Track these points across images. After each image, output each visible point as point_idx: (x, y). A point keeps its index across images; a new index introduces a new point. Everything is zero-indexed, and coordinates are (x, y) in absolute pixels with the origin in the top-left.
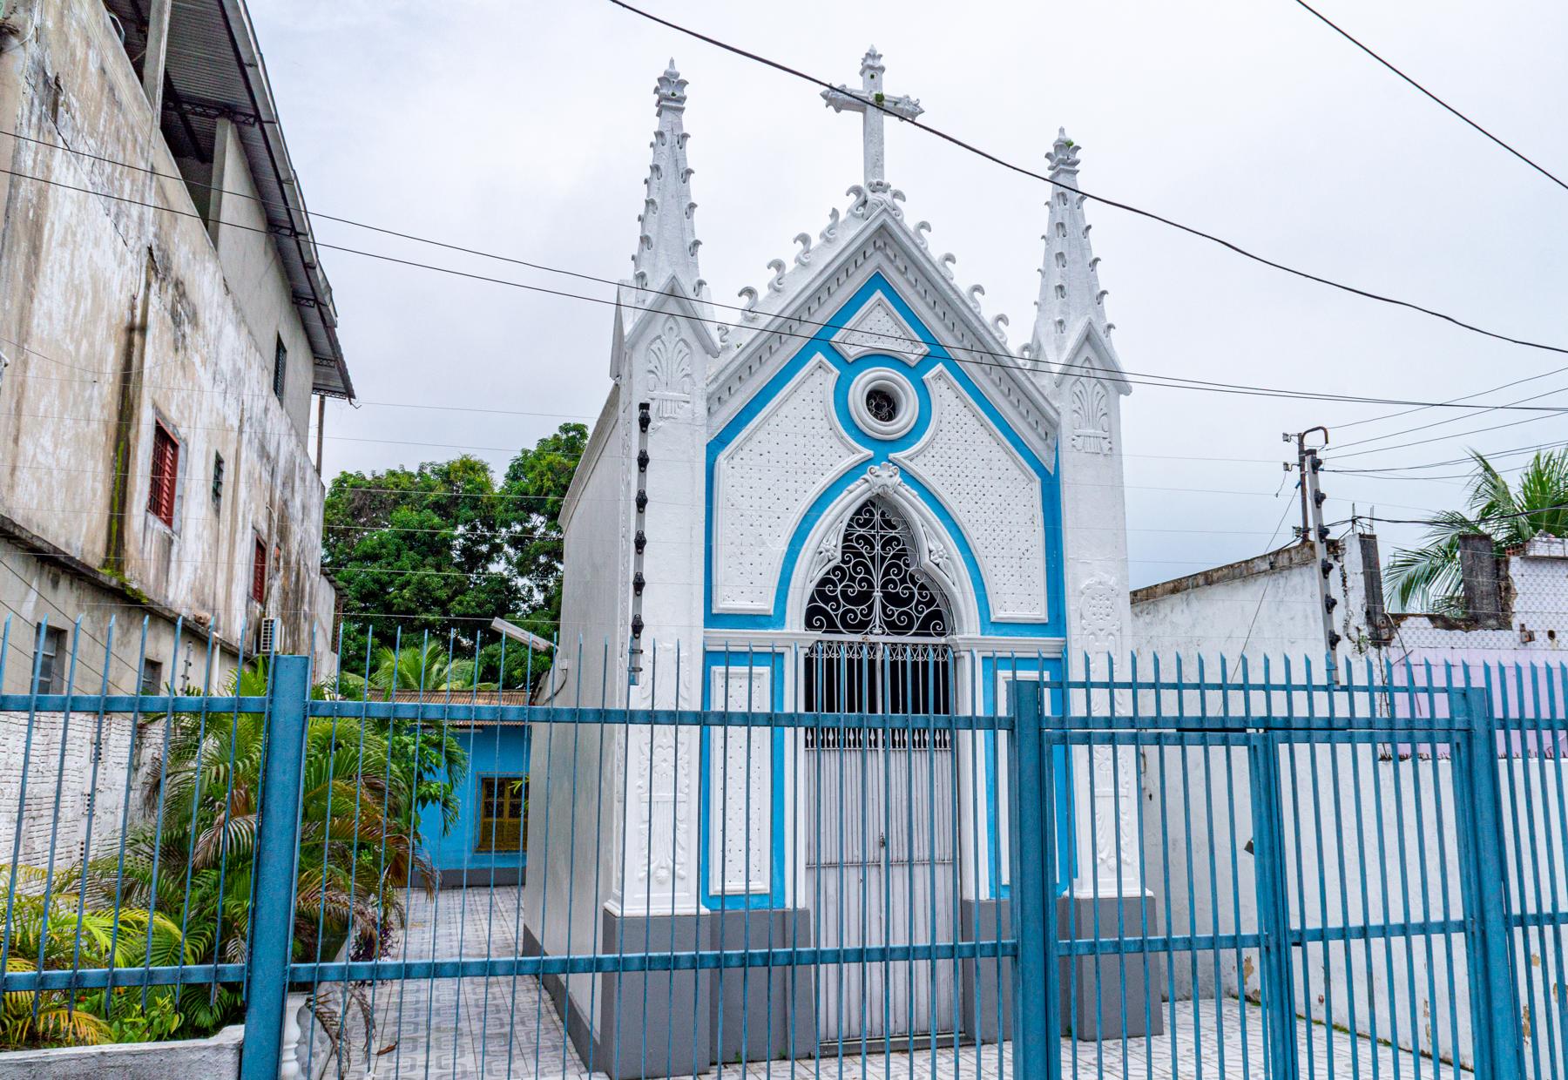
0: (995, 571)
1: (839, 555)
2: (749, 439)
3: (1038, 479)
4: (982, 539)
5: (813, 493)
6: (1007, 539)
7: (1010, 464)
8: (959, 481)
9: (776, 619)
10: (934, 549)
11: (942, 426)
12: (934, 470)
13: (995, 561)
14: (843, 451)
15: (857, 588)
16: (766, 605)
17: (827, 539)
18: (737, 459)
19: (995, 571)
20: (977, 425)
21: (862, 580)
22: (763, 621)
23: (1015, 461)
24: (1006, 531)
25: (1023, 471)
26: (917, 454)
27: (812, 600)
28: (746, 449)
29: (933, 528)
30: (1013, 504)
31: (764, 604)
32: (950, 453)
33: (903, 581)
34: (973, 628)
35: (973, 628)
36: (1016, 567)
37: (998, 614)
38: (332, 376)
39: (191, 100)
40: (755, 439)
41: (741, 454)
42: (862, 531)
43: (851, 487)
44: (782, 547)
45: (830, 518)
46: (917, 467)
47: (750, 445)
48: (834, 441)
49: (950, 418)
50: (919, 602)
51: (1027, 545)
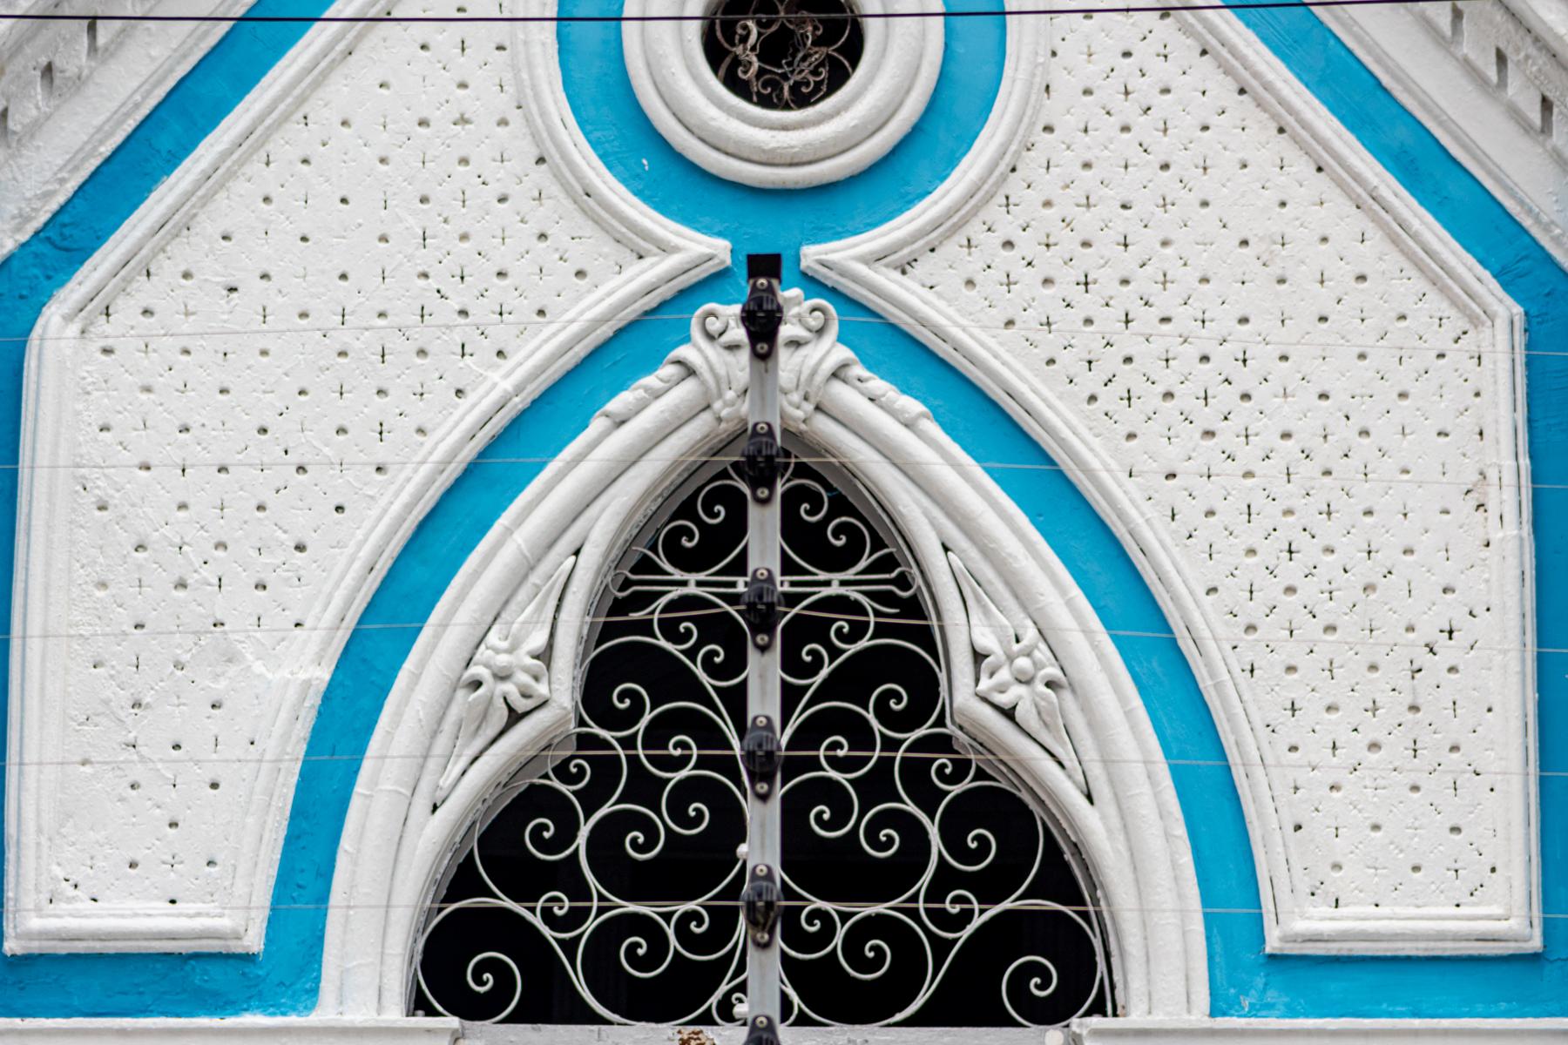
0: (1291, 729)
1: (563, 690)
2: (177, 225)
3: (1506, 308)
4: (1232, 592)
5: (453, 433)
6: (1349, 587)
7: (1375, 254)
8: (1127, 343)
9: (277, 969)
10: (1017, 649)
11: (1052, 110)
12: (1009, 305)
13: (1293, 688)
14: (593, 248)
15: (663, 821)
16: (234, 912)
17: (516, 634)
18: (126, 311)
19: (1291, 729)
20: (1221, 90)
21: (686, 791)
22: (218, 976)
23: (1398, 235)
24: (1350, 550)
25: (1438, 278)
26: (932, 240)
27: (462, 881)
28: (167, 270)
29: (989, 553)
30: (1384, 431)
31: (229, 907)
32: (1086, 222)
33: (876, 786)
34: (1170, 983)
35: (1170, 983)
36: (1392, 707)
37: (1297, 919)
38: (1189, 1011)
39: (360, 37)
40: (208, 226)
41: (145, 292)
42: (692, 584)
43: (620, 402)
44: (307, 667)
45: (521, 541)
46: (929, 300)
47: (183, 253)
48: (558, 213)
49: (1091, 72)
50: (946, 880)
51: (1451, 610)
